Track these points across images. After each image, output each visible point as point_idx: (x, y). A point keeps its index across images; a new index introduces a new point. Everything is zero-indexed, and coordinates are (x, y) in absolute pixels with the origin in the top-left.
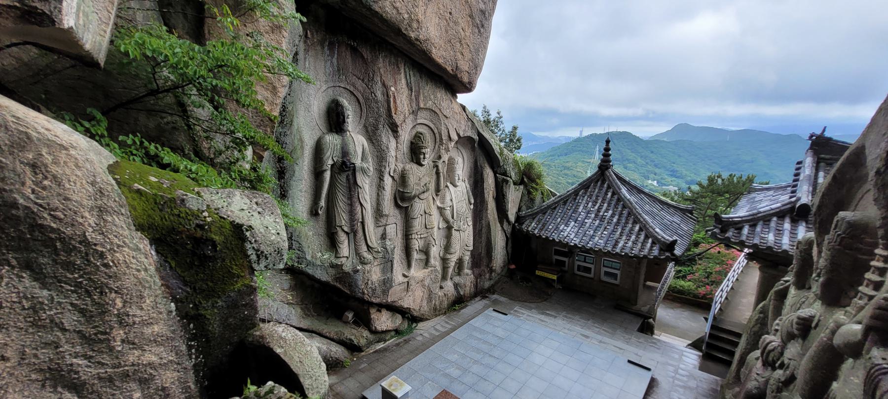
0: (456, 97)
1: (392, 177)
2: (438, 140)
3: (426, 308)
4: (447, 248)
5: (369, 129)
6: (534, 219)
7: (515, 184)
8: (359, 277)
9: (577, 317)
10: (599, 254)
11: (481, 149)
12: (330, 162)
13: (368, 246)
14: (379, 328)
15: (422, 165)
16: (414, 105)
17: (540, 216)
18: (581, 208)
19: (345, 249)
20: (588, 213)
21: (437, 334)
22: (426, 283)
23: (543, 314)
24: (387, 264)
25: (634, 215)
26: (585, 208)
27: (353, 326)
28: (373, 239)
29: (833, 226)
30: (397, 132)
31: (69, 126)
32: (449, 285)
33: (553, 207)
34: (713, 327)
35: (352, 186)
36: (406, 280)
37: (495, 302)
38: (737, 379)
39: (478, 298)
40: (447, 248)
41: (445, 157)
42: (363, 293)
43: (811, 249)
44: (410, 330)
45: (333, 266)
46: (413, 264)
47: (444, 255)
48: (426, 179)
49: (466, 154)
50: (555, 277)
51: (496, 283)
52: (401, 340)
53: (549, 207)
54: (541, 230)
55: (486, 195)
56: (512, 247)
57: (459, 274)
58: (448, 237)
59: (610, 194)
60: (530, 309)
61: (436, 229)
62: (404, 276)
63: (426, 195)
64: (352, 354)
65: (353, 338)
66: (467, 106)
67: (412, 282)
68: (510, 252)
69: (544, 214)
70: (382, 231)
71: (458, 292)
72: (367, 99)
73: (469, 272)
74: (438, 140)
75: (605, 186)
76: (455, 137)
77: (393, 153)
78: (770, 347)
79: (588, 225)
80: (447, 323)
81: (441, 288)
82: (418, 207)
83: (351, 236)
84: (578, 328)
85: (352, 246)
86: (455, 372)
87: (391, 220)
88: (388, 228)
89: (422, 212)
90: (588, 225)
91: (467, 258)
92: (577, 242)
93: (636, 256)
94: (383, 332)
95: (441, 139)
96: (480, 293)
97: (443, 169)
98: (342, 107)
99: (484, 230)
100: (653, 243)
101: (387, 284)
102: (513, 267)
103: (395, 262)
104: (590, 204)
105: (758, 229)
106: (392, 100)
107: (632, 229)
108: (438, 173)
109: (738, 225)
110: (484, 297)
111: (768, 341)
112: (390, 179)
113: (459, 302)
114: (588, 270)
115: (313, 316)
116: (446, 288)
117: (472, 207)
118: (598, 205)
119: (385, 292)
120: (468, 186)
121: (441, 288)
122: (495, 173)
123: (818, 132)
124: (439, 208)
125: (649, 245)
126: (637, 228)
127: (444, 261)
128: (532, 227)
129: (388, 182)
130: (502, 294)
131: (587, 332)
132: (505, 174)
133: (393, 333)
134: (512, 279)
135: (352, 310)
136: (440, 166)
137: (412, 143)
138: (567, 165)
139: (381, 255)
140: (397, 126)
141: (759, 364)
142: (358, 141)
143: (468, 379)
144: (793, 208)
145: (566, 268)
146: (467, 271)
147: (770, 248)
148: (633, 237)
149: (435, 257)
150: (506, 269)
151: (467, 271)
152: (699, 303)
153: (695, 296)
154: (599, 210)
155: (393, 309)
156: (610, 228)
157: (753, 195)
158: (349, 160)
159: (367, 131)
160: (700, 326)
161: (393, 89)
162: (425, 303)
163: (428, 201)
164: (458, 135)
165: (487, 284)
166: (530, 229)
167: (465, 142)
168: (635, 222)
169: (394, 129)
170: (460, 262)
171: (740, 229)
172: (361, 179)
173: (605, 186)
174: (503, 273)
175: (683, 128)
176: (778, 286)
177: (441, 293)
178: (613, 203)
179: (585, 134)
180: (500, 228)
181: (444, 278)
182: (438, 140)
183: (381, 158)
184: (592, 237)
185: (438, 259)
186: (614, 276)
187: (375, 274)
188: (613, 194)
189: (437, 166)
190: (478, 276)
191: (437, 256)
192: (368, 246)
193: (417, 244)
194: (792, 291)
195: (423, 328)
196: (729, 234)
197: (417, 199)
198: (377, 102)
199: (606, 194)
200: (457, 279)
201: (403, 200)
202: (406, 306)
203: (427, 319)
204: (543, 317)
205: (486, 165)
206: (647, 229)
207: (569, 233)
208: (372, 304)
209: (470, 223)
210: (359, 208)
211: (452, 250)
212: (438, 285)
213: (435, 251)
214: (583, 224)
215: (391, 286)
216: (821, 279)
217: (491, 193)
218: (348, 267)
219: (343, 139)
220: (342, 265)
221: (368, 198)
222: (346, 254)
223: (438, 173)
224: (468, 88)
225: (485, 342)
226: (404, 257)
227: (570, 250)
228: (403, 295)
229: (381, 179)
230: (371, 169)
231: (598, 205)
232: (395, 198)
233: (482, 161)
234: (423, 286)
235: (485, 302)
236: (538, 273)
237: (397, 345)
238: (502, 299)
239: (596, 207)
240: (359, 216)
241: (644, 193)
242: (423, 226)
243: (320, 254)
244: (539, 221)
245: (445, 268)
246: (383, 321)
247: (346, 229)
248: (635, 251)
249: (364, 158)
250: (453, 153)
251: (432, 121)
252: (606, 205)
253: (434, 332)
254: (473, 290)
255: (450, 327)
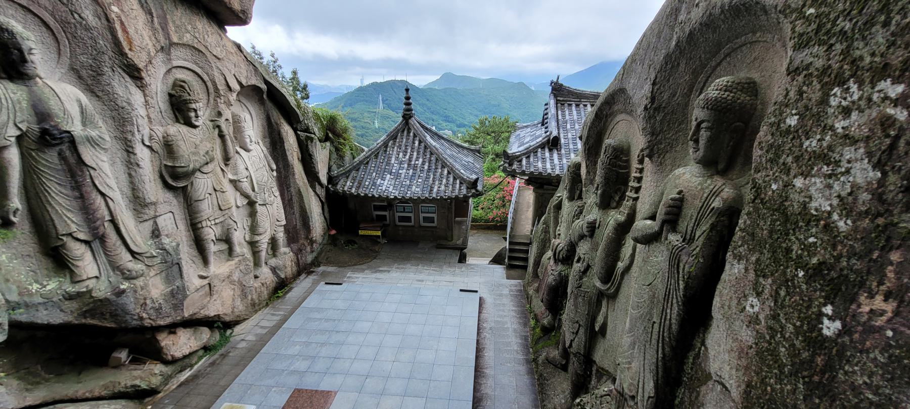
0: (225, 31)
1: (149, 147)
2: (211, 90)
3: (240, 307)
4: (254, 229)
5: (84, 73)
6: (347, 177)
7: (320, 141)
8: (130, 303)
9: (409, 266)
10: (416, 202)
11: (274, 100)
12: (13, 132)
13: (133, 253)
14: (178, 354)
15: (195, 127)
16: (162, 39)
17: (354, 173)
18: (393, 159)
19: (87, 264)
20: (401, 163)
21: (265, 331)
22: (235, 278)
23: (376, 272)
24: (171, 267)
25: (441, 160)
26: (397, 159)
27: (133, 367)
28: (139, 239)
29: (603, 151)
30: (141, 79)
31: (526, 312)
32: (265, 273)
33: (365, 162)
34: (510, 243)
35: (76, 171)
36: (206, 282)
37: (324, 275)
38: (536, 275)
39: (304, 276)
40: (254, 229)
41: (227, 114)
42: (141, 319)
43: (579, 169)
44: (225, 340)
45: (70, 297)
46: (212, 258)
47: (251, 238)
48: (205, 146)
49: (254, 108)
50: (379, 233)
51: (319, 254)
52: (216, 356)
53: (361, 162)
54: (358, 188)
55: (290, 158)
56: (330, 212)
57: (274, 255)
58: (253, 214)
59: (417, 143)
60: (363, 270)
61: (234, 208)
62: (202, 277)
63: (210, 167)
64: (141, 403)
65: (137, 382)
66: (243, 45)
67: (215, 282)
68: (328, 217)
69: (358, 170)
70: (149, 225)
71: (278, 276)
72: (64, 23)
73: (287, 250)
74: (213, 91)
75: (412, 134)
76: (236, 87)
77: (142, 112)
78: (559, 249)
79: (403, 176)
80: (273, 315)
81: (256, 277)
82: (202, 185)
83: (96, 245)
84: (412, 275)
85: (102, 259)
86: (302, 365)
87: (162, 209)
88: (160, 221)
89: (211, 190)
90: (403, 176)
91: (281, 236)
92: (396, 195)
93: (449, 198)
94: (185, 357)
95: (216, 90)
96: (303, 269)
97: (228, 130)
98: (12, 33)
99: (295, 199)
100: (461, 183)
101: (177, 296)
102: (333, 232)
103: (184, 263)
104: (401, 154)
105: (532, 159)
106: (118, 26)
107: (442, 174)
108: (221, 136)
109: (517, 158)
110: (310, 273)
111: (556, 243)
112: (147, 152)
113: (282, 286)
114: (408, 219)
115: (47, 380)
116: (262, 277)
117: (275, 174)
118: (408, 154)
119: (178, 307)
120: (264, 149)
121: (256, 277)
122: (295, 130)
123: (555, 80)
124: (231, 181)
125: (458, 186)
126: (446, 172)
127: (253, 245)
128: (347, 186)
129: (143, 155)
130: (329, 263)
131: (421, 277)
132: (307, 130)
133: (201, 353)
134: (335, 245)
135: (123, 346)
136: (223, 127)
137: (170, 95)
138: (353, 116)
139: (158, 260)
140: (138, 70)
141: (552, 262)
142: (68, 99)
143: (320, 365)
144: (549, 140)
145: (388, 222)
146: (283, 249)
147: (541, 173)
148: (444, 181)
149: (240, 244)
150: (327, 237)
151: (283, 249)
152: (497, 226)
153: (487, 221)
154: (410, 160)
155: (192, 323)
156: (424, 175)
157: (518, 132)
158: (56, 127)
159: (80, 77)
160: (498, 244)
161: (115, 9)
162: (238, 302)
163: (216, 174)
164: (240, 84)
165: (310, 258)
166: (346, 189)
167: (251, 93)
168: (443, 167)
169: (134, 73)
170: (273, 242)
171: (521, 161)
172: (88, 155)
173: (412, 134)
174: (325, 242)
175: (448, 77)
176: (554, 201)
177: (257, 284)
178: (422, 151)
179: (367, 82)
180: (313, 194)
181: (257, 264)
182: (213, 91)
183: (121, 121)
184: (410, 186)
185: (245, 243)
186: (431, 220)
187: (155, 288)
188: (420, 142)
189: (219, 127)
190: (298, 253)
191: (243, 241)
192: (133, 253)
193: (210, 233)
194: (566, 204)
195: (244, 334)
196: (515, 167)
197: (198, 174)
198: (88, 28)
199: (414, 143)
200: (273, 262)
201: (176, 179)
202: (212, 314)
203: (245, 320)
204: (378, 275)
205: (283, 121)
206: (454, 172)
207: (387, 186)
208: (160, 329)
209: (277, 194)
210: (99, 201)
211: (261, 230)
212: (252, 275)
213: (239, 236)
214: (398, 175)
215: (185, 297)
216: (599, 192)
217: (295, 154)
218: (102, 290)
219: (31, 93)
220: (89, 292)
221: (112, 183)
222: (95, 273)
223: (221, 136)
224: (241, 19)
225: (327, 320)
226: (195, 252)
227: (389, 204)
228: (205, 301)
229: (129, 151)
230: (107, 138)
231: (408, 154)
232: (162, 177)
233: (276, 116)
234: (232, 282)
235: (312, 278)
236: (361, 232)
237: (213, 364)
238: (330, 269)
239: (407, 157)
240: (103, 212)
241: (443, 138)
242: (216, 208)
243: (36, 286)
244: (354, 179)
245: (256, 254)
246: (181, 344)
247: (82, 236)
248: (449, 193)
249: (86, 120)
250: (237, 109)
251: (197, 64)
252: (415, 154)
253: (260, 331)
254: (295, 269)
255: (278, 318)
